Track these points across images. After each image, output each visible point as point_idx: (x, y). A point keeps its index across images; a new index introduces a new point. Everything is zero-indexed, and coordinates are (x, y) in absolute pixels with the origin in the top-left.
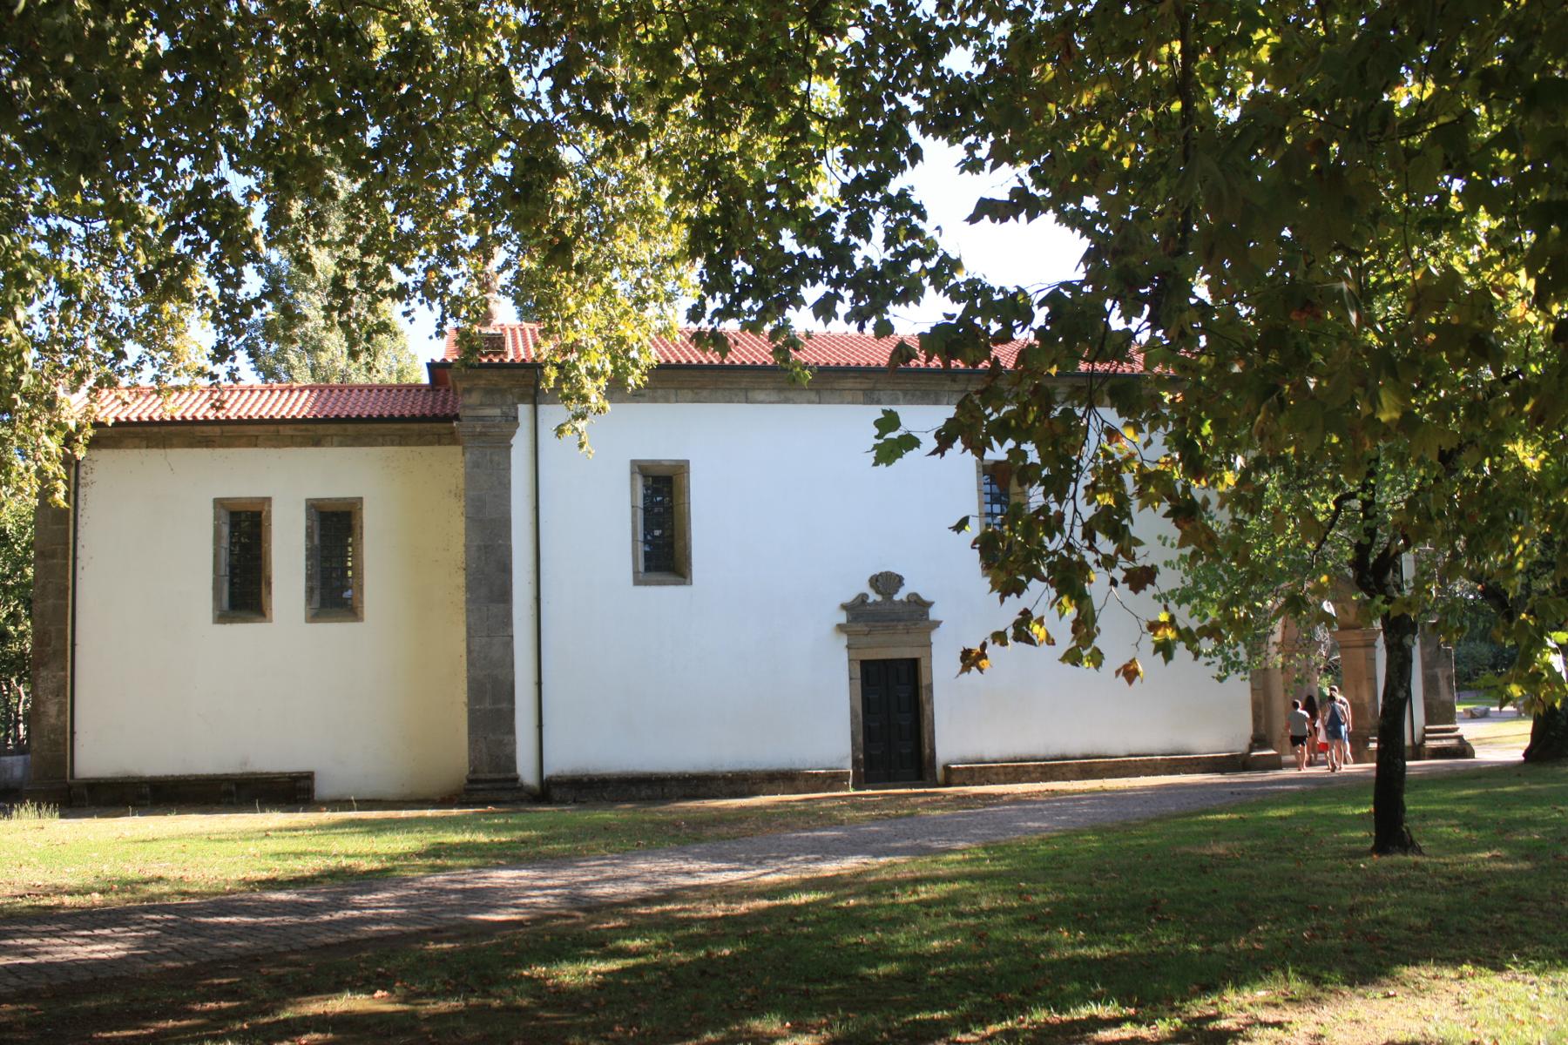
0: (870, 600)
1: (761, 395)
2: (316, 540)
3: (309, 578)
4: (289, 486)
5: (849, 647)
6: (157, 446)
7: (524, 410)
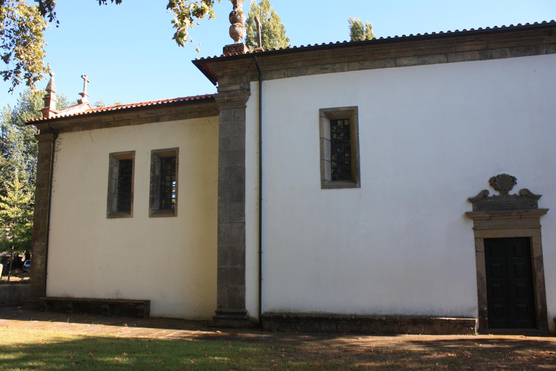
0: (490, 195)
1: (406, 61)
2: (157, 172)
3: (152, 192)
4: (143, 143)
5: (474, 229)
6: (87, 129)
7: (254, 85)
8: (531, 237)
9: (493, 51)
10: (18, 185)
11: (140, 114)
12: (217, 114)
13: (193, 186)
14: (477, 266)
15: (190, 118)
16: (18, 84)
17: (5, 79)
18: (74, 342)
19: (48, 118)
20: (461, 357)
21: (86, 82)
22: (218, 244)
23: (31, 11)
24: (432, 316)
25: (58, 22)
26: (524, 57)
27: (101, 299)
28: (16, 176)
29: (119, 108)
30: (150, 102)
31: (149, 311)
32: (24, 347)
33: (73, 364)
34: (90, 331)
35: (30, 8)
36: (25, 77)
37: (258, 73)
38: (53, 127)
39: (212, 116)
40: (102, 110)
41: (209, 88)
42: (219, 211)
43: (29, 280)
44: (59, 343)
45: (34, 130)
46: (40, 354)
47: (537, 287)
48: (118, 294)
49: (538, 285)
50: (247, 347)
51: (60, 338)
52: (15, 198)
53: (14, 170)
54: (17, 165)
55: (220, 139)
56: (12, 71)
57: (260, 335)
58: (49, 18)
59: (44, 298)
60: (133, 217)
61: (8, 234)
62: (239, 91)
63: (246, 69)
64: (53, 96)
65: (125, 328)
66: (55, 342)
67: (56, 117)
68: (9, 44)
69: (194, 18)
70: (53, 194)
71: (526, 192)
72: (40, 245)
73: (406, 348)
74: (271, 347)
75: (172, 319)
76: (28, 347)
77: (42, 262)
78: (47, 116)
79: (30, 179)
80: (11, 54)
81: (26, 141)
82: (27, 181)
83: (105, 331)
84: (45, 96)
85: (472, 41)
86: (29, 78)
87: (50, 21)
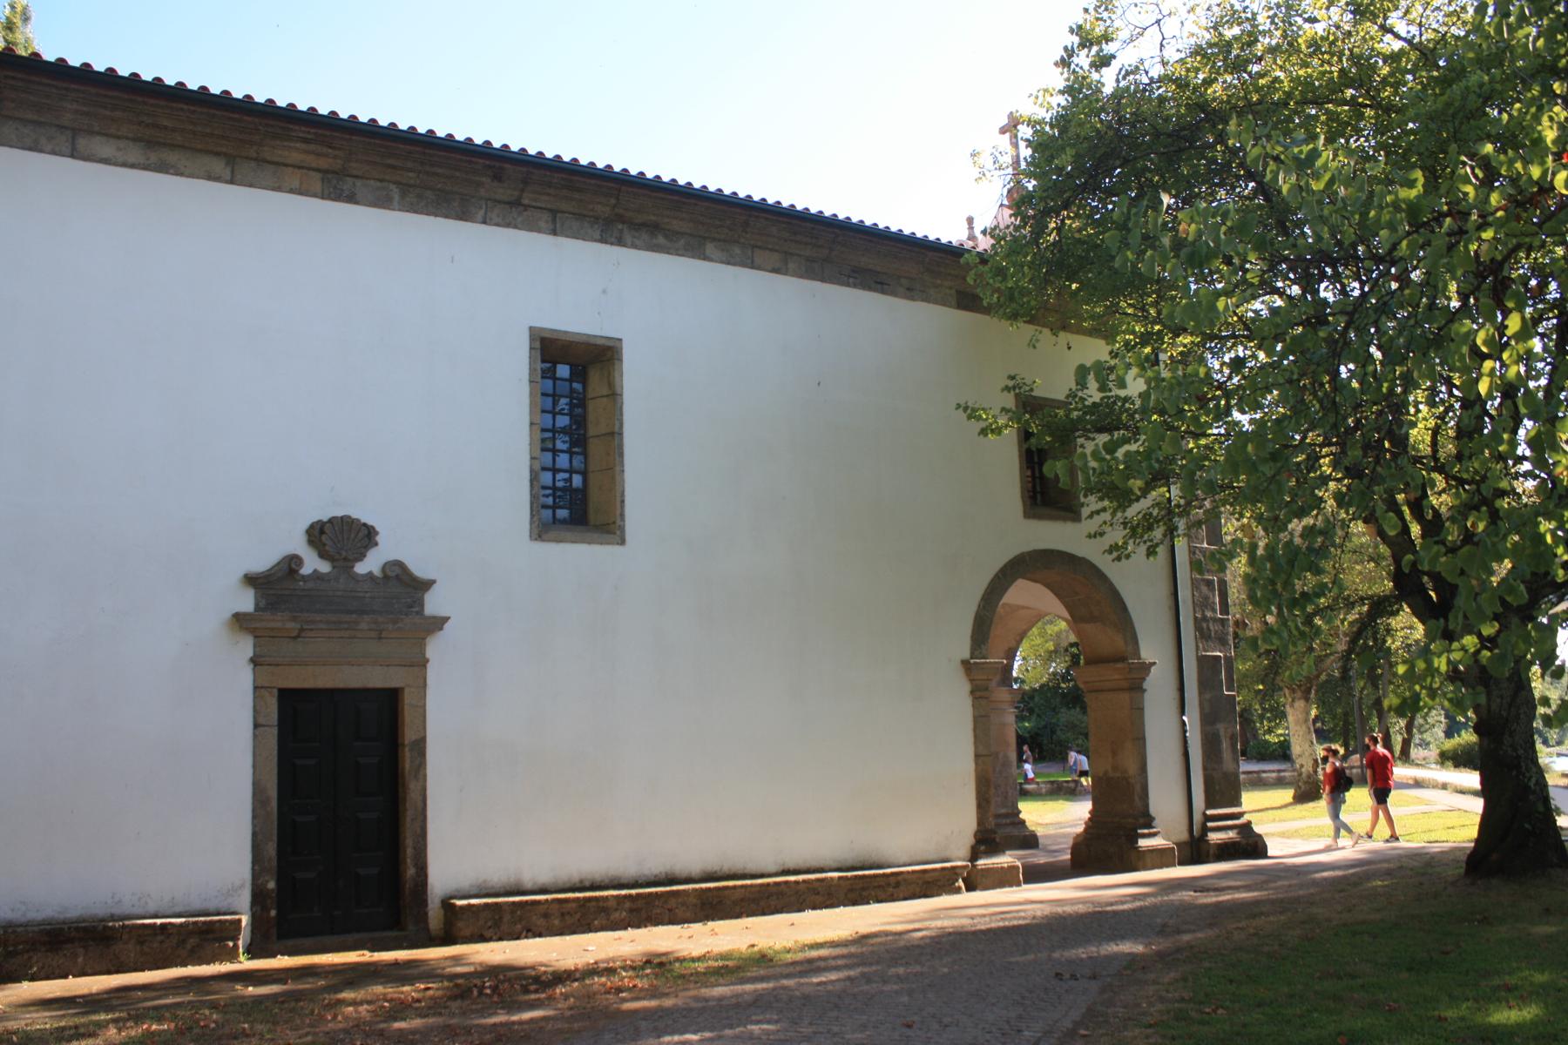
0: (306, 570)
1: (107, 148)
5: (255, 661)
8: (402, 689)
9: (359, 183)
14: (254, 766)
20: (190, 1029)
24: (113, 918)
26: (432, 218)
47: (408, 819)
49: (410, 814)
71: (398, 570)
73: (12, 1025)
85: (306, 141)
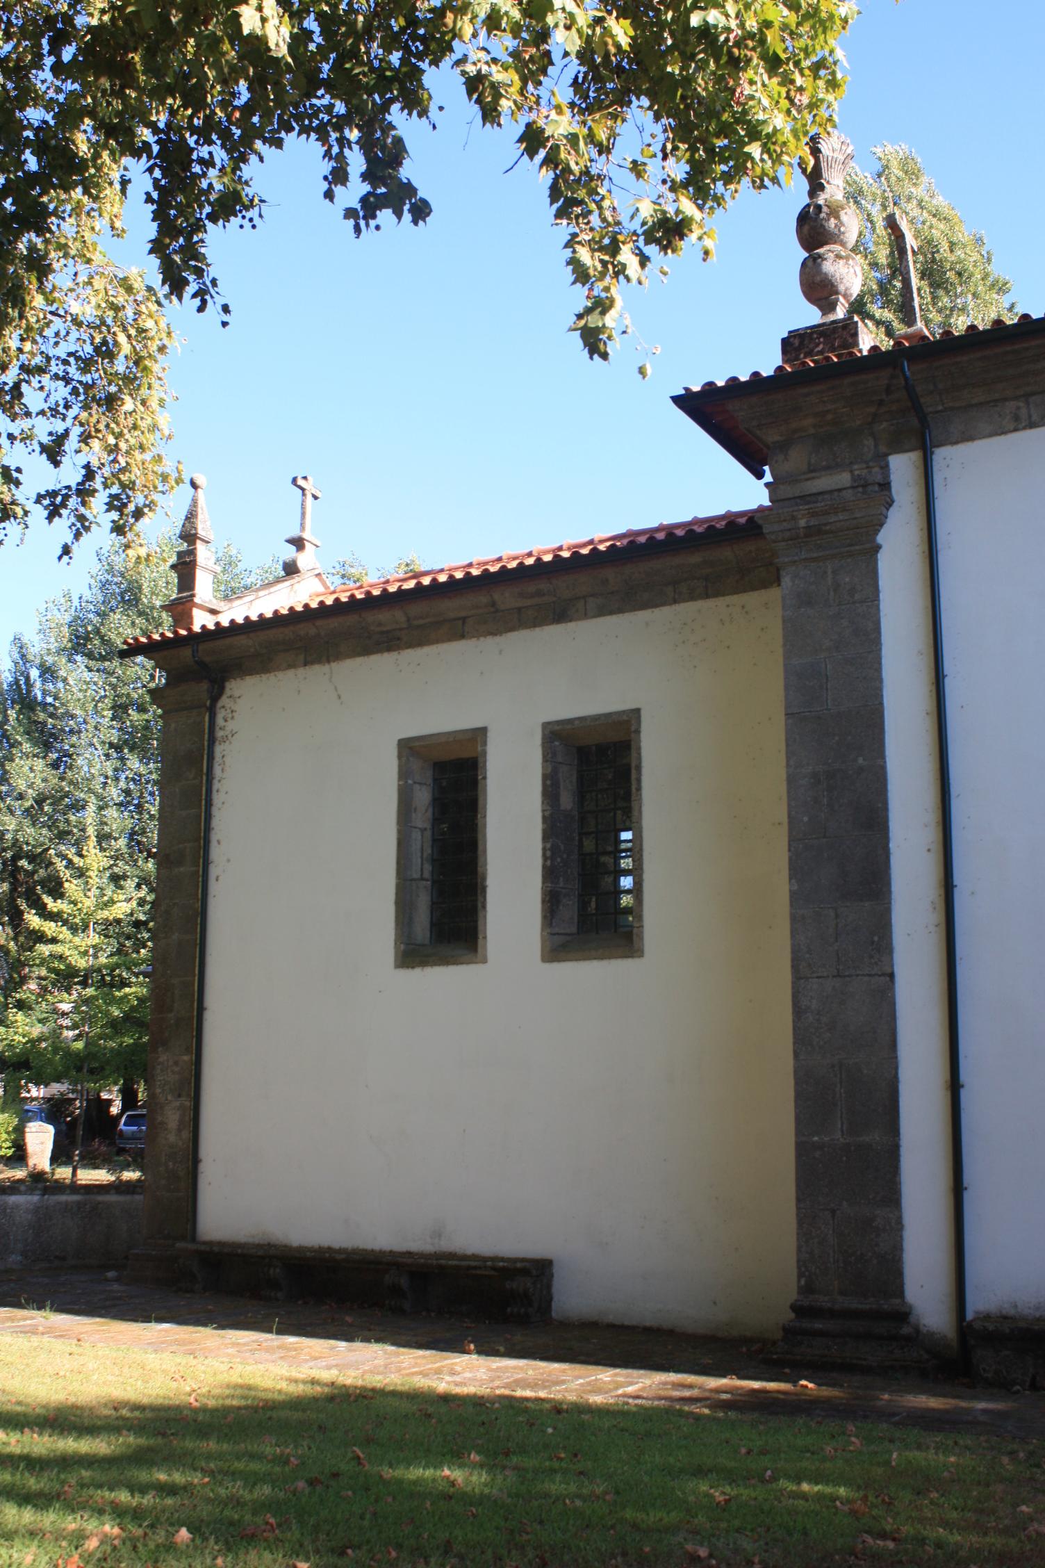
2: (567, 801)
3: (550, 873)
4: (511, 699)
6: (318, 661)
7: (902, 467)
10: (95, 859)
11: (496, 597)
12: (772, 579)
13: (698, 846)
15: (675, 602)
16: (87, 529)
17: (50, 518)
18: (296, 1404)
19: (190, 630)
21: (309, 497)
22: (796, 1055)
23: (129, 289)
25: (226, 309)
27: (382, 1252)
28: (91, 831)
29: (426, 581)
30: (530, 554)
31: (551, 1299)
32: (137, 1413)
33: (301, 1484)
34: (348, 1366)
35: (125, 279)
36: (110, 507)
37: (915, 422)
38: (207, 659)
39: (754, 589)
40: (368, 593)
41: (736, 489)
42: (794, 933)
43: (139, 1180)
44: (246, 1407)
45: (142, 671)
46: (189, 1444)
48: (438, 1234)
50: (919, 1447)
51: (249, 1388)
52: (88, 903)
53: (83, 807)
54: (90, 791)
55: (788, 671)
56: (68, 488)
57: (963, 1404)
58: (197, 302)
59: (191, 1246)
60: (484, 961)
61: (66, 1022)
62: (848, 494)
63: (872, 409)
64: (204, 555)
65: (466, 1357)
66: (235, 1403)
67: (217, 624)
68: (62, 403)
69: (652, 250)
70: (214, 887)
72: (176, 1063)
74: (1012, 1453)
75: (628, 1327)
76: (149, 1414)
77: (181, 1122)
78: (188, 624)
79: (132, 834)
80: (67, 431)
81: (120, 710)
82: (122, 843)
83: (399, 1370)
84: (180, 554)
86: (121, 509)
87: (201, 309)
